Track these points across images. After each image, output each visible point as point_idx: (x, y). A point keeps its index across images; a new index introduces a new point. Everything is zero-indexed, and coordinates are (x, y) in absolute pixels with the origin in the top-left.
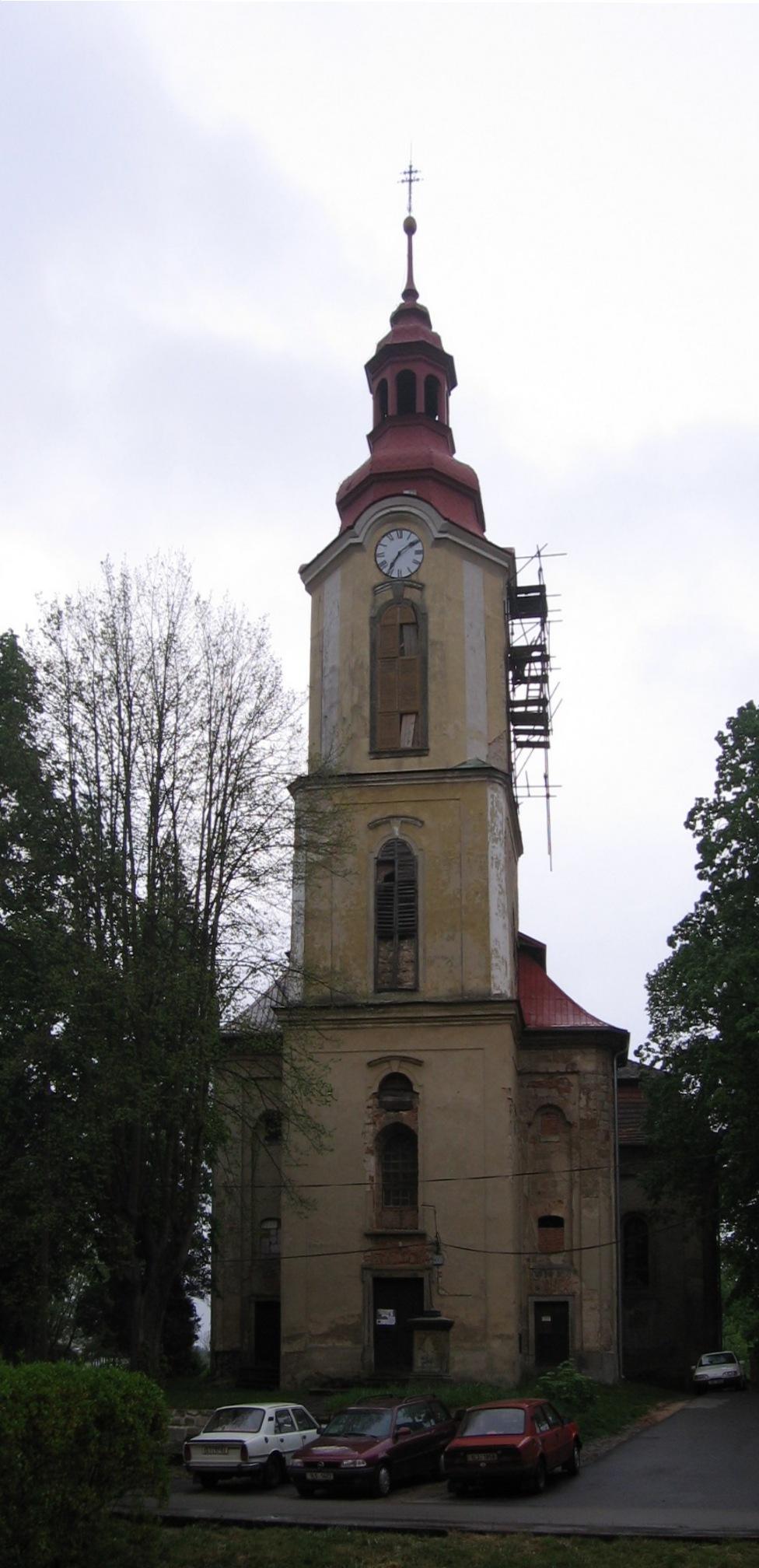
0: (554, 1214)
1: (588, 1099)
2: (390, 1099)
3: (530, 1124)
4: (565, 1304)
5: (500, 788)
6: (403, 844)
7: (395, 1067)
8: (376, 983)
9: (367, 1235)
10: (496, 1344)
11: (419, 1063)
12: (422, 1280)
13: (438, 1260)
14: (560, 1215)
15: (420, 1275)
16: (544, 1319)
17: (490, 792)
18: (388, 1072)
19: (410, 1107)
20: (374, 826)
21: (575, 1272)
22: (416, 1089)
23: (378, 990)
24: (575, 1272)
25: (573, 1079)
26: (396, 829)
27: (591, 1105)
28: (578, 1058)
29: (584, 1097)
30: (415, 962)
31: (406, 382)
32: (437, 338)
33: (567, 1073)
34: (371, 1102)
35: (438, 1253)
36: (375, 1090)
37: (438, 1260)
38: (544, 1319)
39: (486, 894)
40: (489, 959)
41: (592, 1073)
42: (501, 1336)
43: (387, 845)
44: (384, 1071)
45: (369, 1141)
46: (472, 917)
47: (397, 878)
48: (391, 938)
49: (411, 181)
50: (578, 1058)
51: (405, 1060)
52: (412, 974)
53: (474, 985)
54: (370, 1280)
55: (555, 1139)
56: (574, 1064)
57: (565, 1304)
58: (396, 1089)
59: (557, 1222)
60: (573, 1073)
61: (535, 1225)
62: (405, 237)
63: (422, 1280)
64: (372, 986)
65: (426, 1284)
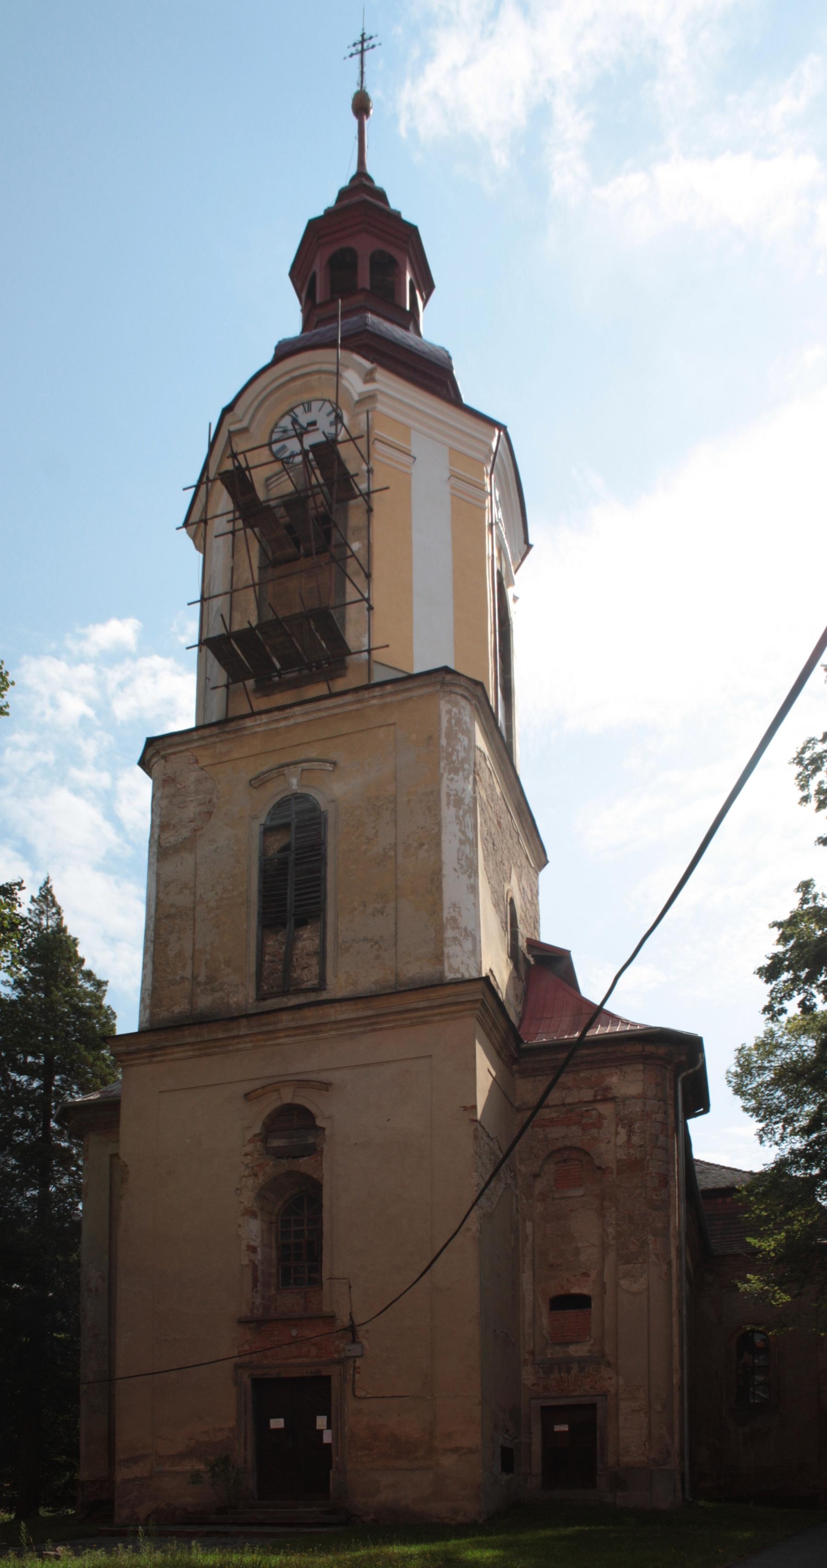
0: (575, 1290)
1: (630, 1133)
2: (277, 1143)
3: (536, 1176)
4: (593, 1407)
5: (463, 702)
6: (305, 797)
7: (287, 1096)
8: (258, 988)
9: (243, 1322)
10: (448, 1461)
11: (326, 1086)
12: (329, 1378)
13: (355, 1350)
14: (585, 1291)
15: (325, 1372)
16: (558, 1428)
17: (444, 706)
18: (276, 1104)
19: (313, 1151)
20: (258, 782)
21: (609, 1364)
22: (319, 1122)
23: (261, 997)
24: (609, 1364)
25: (606, 1109)
26: (294, 781)
27: (635, 1140)
28: (614, 1080)
29: (623, 1132)
30: (321, 954)
31: (342, 267)
32: (452, 367)
33: (595, 1101)
34: (249, 1148)
35: (354, 1341)
36: (257, 1129)
37: (355, 1350)
38: (558, 1428)
39: (437, 844)
40: (440, 930)
41: (638, 1097)
42: (456, 1450)
43: (279, 805)
44: (272, 1103)
45: (248, 1198)
46: (424, 896)
47: (293, 848)
48: (284, 925)
49: (362, 52)
50: (614, 1080)
51: (303, 1084)
52: (315, 970)
53: (415, 969)
54: (248, 1382)
55: (578, 1192)
56: (608, 1089)
57: (593, 1407)
58: (292, 1130)
59: (582, 1302)
60: (605, 1100)
61: (544, 1308)
62: (355, 122)
63: (329, 1378)
64: (252, 993)
65: (335, 1382)
